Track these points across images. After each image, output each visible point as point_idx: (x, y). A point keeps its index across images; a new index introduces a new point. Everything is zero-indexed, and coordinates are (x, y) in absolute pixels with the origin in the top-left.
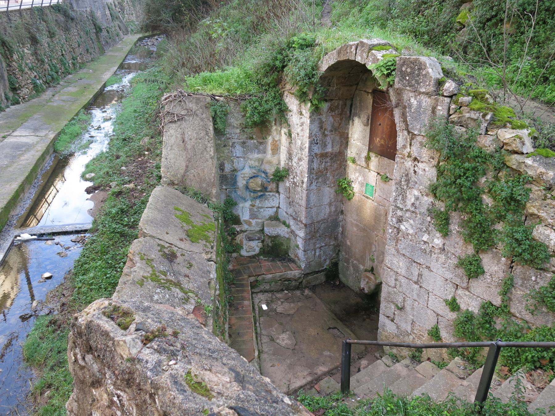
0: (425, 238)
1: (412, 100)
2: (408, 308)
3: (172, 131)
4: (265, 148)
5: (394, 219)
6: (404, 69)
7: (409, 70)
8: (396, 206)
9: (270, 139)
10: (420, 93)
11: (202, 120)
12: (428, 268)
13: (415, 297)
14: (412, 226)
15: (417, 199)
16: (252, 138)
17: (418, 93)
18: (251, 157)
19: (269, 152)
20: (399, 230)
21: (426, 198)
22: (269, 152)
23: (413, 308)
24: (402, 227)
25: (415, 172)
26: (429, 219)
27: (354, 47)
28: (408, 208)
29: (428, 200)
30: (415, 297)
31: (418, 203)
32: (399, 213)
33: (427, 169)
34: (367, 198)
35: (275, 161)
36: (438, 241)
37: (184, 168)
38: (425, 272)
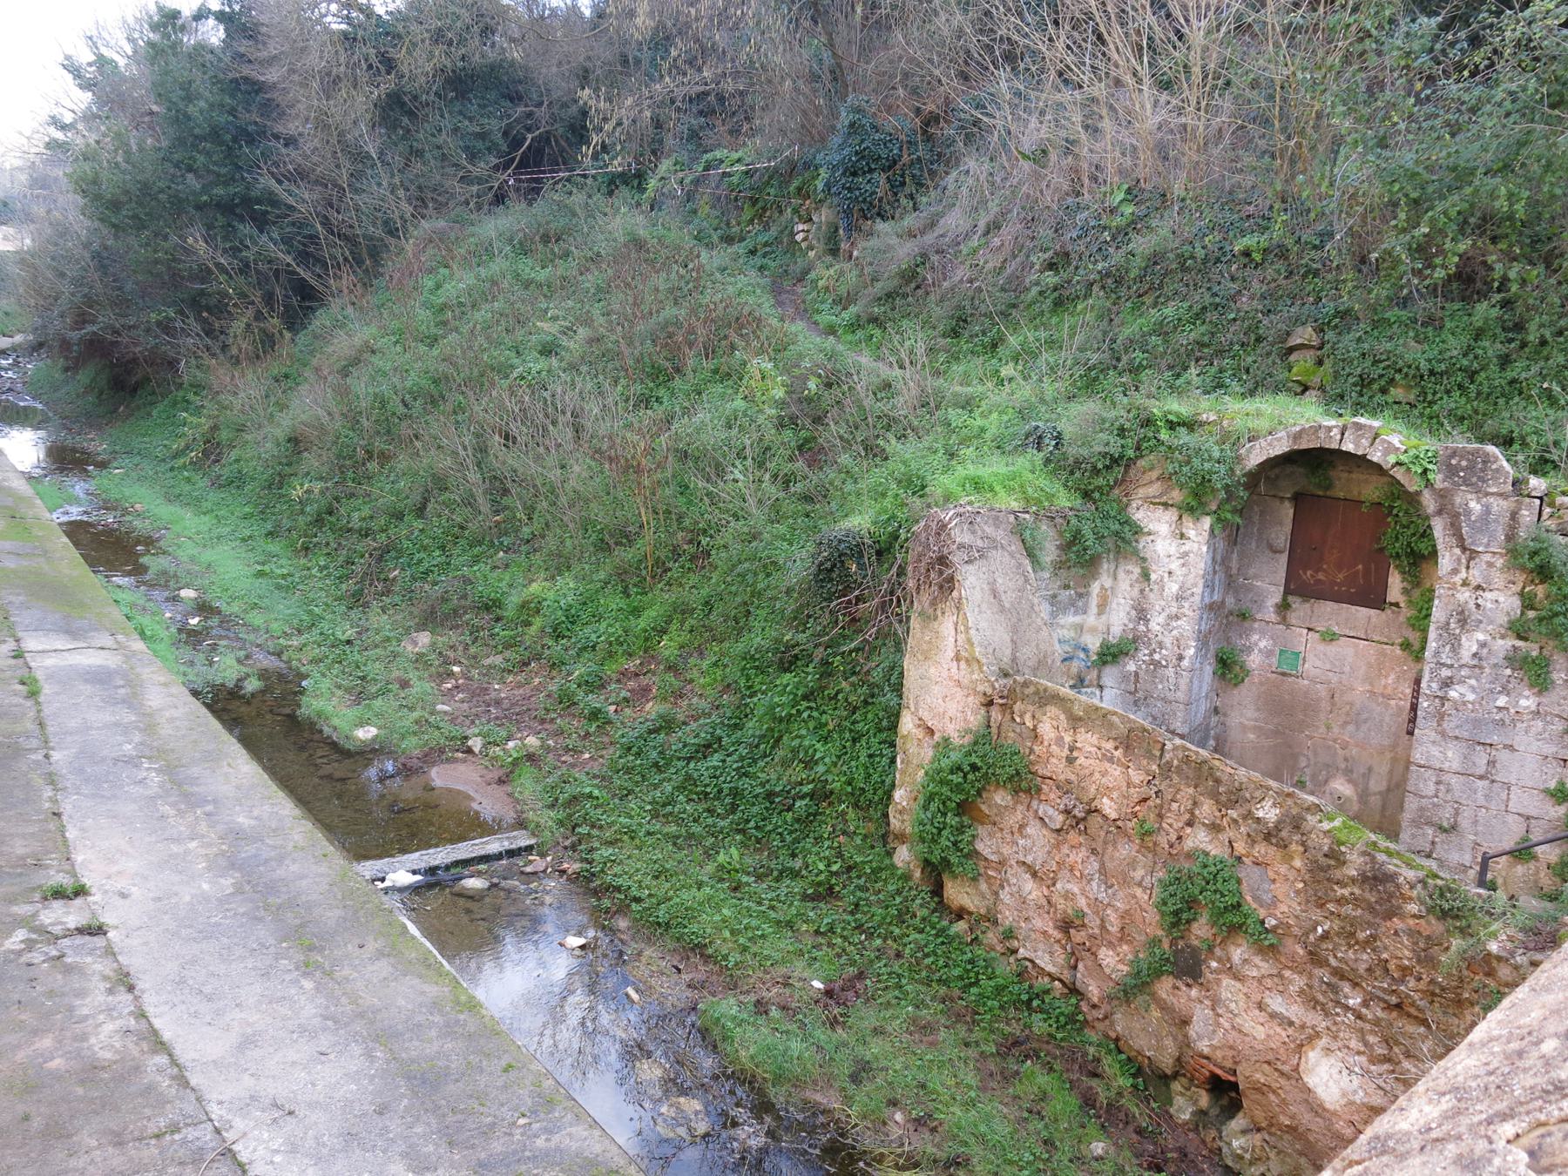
0: (1502, 701)
1: (1472, 504)
2: (1464, 823)
3: (972, 579)
4: (1086, 605)
5: (1434, 685)
6: (1454, 462)
7: (1464, 463)
8: (1438, 663)
9: (1095, 588)
10: (1487, 494)
11: (1012, 555)
12: (1511, 748)
13: (1481, 801)
14: (1473, 689)
15: (1483, 645)
16: (1067, 587)
17: (1480, 493)
18: (1062, 622)
19: (1093, 609)
20: (1443, 699)
21: (1501, 642)
22: (1093, 609)
23: (1475, 822)
24: (1453, 694)
25: (1478, 606)
26: (1508, 672)
27: (1335, 431)
28: (1463, 662)
29: (1504, 645)
30: (1481, 801)
31: (1485, 651)
32: (1445, 673)
33: (1501, 599)
34: (1284, 674)
35: (1102, 628)
36: (1528, 702)
37: (1010, 644)
38: (1503, 756)
